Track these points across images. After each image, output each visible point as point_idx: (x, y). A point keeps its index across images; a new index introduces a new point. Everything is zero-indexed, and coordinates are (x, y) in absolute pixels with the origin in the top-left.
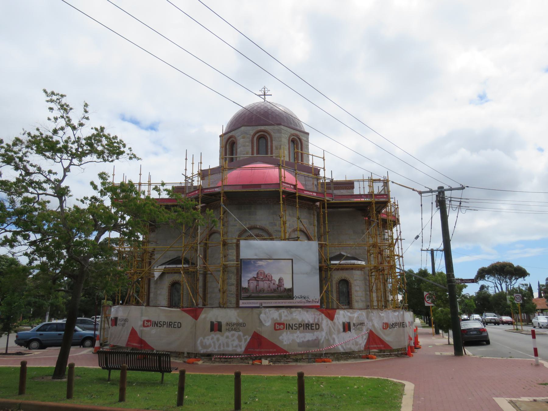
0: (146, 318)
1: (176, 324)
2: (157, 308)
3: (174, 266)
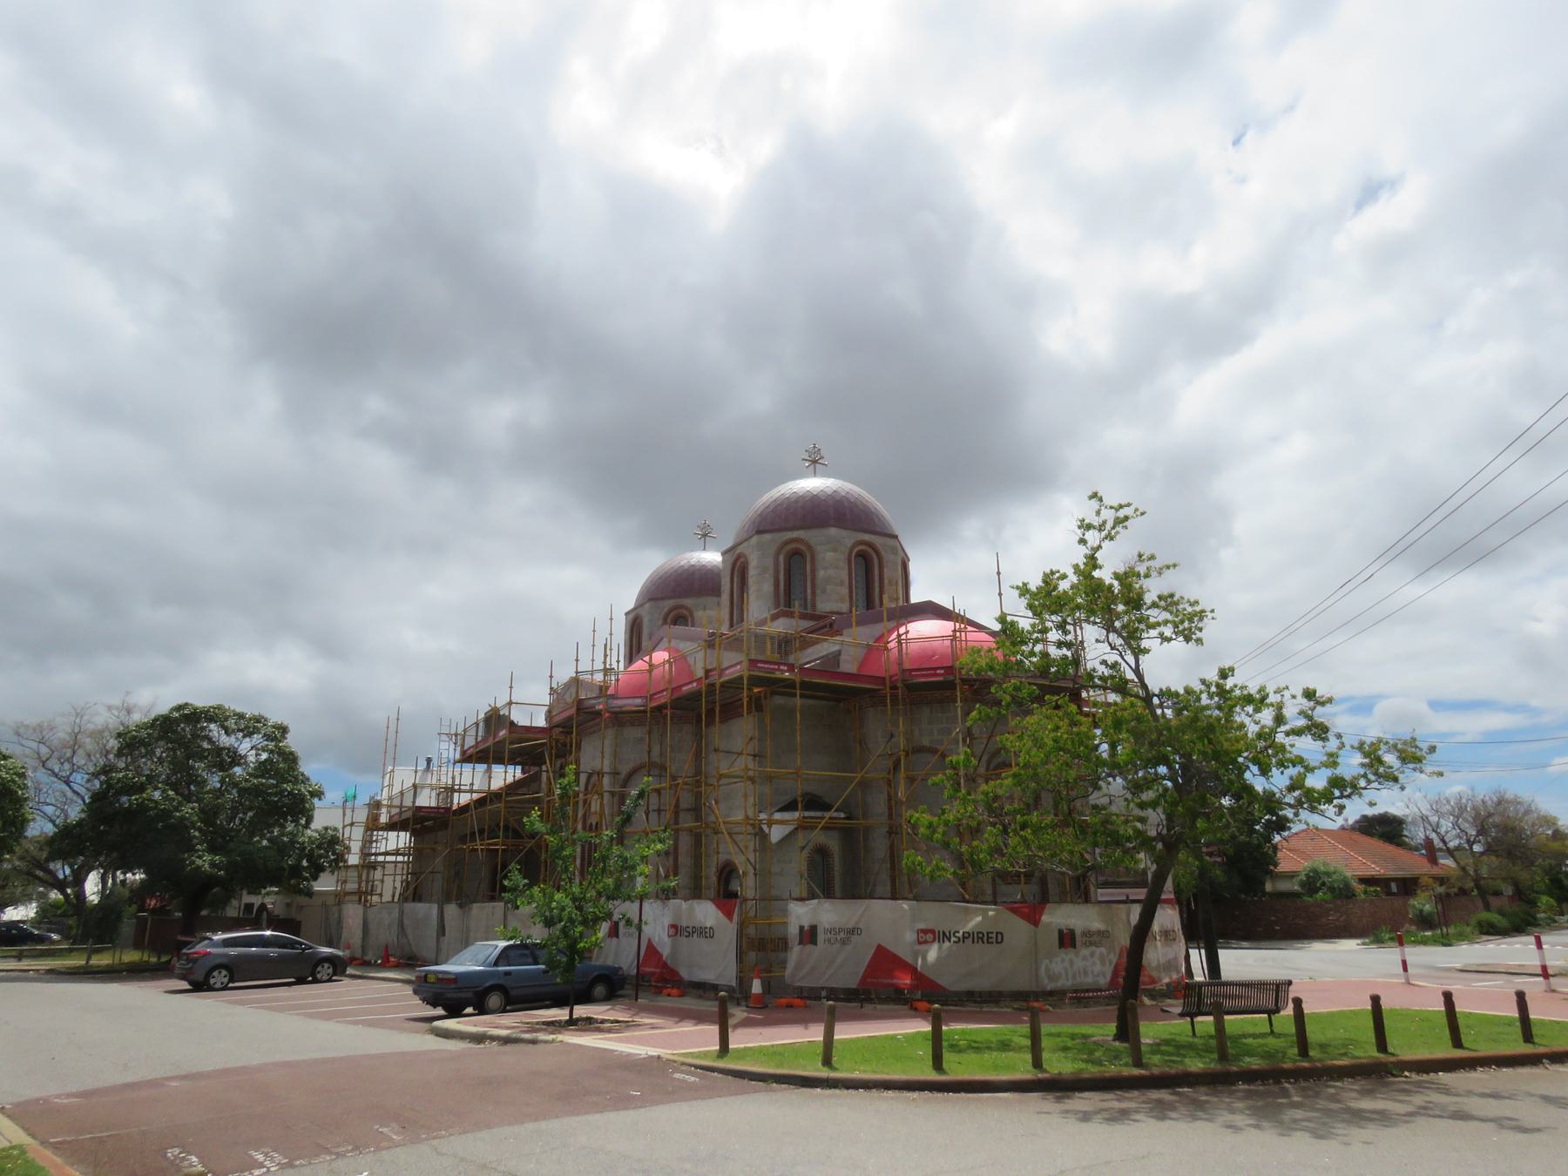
1: (994, 935)
3: (148, 933)
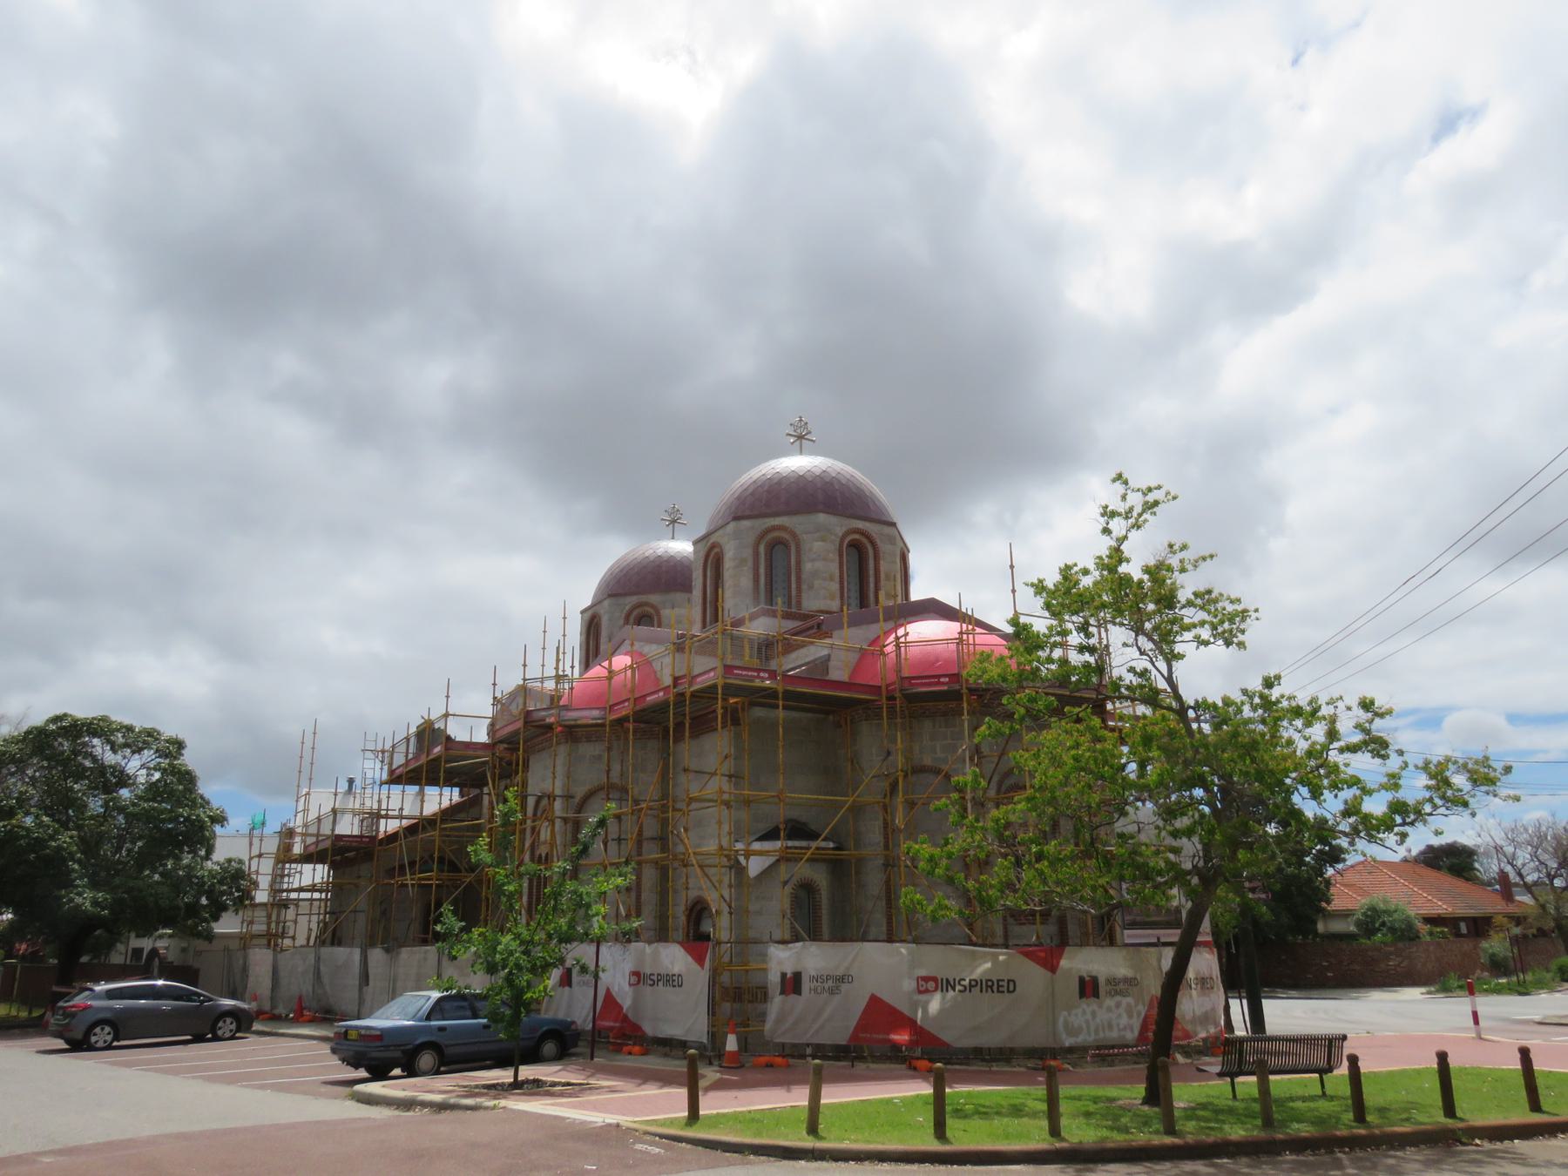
0: (923, 973)
1: (1005, 984)
2: (948, 946)
